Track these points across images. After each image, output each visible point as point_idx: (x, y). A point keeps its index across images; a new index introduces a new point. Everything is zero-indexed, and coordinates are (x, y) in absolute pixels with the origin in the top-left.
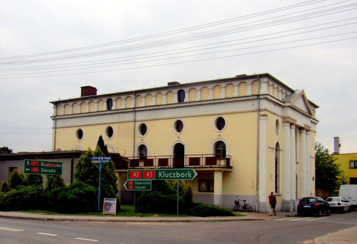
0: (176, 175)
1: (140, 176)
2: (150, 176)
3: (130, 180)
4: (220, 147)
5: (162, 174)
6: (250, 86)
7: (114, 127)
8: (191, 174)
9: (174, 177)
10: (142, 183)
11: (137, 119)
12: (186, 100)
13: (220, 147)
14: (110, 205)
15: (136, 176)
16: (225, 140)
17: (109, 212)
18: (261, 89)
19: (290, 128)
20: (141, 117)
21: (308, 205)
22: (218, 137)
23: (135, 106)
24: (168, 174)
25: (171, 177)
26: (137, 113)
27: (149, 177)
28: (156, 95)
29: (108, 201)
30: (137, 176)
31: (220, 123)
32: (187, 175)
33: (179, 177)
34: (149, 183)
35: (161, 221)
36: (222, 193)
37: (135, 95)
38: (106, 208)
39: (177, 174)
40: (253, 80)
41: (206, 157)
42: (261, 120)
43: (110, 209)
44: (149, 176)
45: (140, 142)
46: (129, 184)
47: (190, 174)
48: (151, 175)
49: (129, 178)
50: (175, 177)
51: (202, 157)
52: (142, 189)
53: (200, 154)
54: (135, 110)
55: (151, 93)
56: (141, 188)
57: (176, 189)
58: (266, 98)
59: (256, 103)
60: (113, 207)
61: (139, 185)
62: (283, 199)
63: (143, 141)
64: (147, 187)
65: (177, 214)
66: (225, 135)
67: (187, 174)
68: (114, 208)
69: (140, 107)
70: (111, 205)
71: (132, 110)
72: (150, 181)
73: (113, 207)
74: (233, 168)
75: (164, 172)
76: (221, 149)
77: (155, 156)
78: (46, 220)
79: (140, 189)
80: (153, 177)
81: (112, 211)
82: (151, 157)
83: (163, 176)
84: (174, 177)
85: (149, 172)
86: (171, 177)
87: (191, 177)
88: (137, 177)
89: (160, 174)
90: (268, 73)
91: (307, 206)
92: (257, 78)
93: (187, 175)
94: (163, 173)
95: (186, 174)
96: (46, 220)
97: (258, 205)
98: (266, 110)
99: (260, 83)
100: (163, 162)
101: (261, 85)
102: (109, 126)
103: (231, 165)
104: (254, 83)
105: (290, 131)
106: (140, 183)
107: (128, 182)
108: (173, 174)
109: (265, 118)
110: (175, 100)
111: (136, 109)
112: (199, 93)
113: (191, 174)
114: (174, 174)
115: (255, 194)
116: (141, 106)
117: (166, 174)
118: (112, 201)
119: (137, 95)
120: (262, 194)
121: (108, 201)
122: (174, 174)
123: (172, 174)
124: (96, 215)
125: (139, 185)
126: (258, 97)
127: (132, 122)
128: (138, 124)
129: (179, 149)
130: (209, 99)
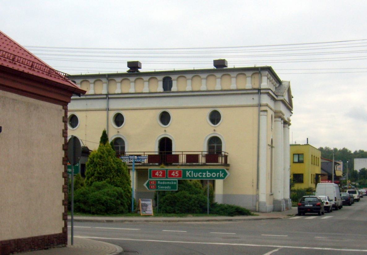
0: (206, 175)
1: (163, 175)
2: (176, 176)
3: (151, 179)
4: (215, 143)
5: (190, 174)
6: (235, 79)
7: (171, 113)
8: (223, 174)
9: (204, 176)
10: (166, 183)
11: (111, 107)
12: (174, 88)
13: (215, 143)
14: (146, 206)
15: (159, 175)
16: (169, 135)
17: (146, 213)
18: (261, 83)
19: (284, 127)
20: (116, 105)
21: (310, 204)
22: (164, 133)
23: (108, 92)
24: (197, 173)
25: (201, 176)
26: (111, 101)
27: (175, 177)
28: (121, 81)
29: (144, 202)
30: (160, 176)
31: (215, 118)
32: (219, 175)
33: (215, 176)
34: (321, 182)
35: (196, 221)
36: (224, 191)
37: (107, 79)
38: (142, 209)
39: (208, 174)
40: (209, 74)
41: (187, 154)
42: (261, 115)
43: (147, 210)
44: (175, 175)
45: (116, 134)
46: (151, 183)
47: (222, 174)
48: (177, 175)
49: (150, 178)
50: (205, 177)
51: (182, 154)
52: (167, 189)
53: (180, 151)
54: (108, 97)
55: (129, 78)
56: (166, 187)
57: (187, 187)
58: (268, 94)
59: (256, 97)
60: (150, 208)
61: (162, 185)
62: (274, 199)
63: (119, 134)
64: (173, 186)
65: (207, 213)
66: (220, 130)
67: (219, 174)
68: (151, 208)
69: (115, 94)
70: (148, 206)
71: (105, 96)
72: (176, 181)
73: (149, 208)
74: (231, 166)
75: (192, 172)
76: (215, 145)
77: (144, 152)
78: (105, 221)
79: (164, 189)
80: (180, 176)
81: (149, 212)
82: (136, 153)
83: (191, 175)
84: (204, 176)
85: (175, 171)
86: (201, 176)
87: (223, 177)
88: (160, 177)
89: (188, 174)
90: (271, 67)
91: (309, 205)
92: (257, 71)
93: (219, 175)
94: (191, 172)
95: (159, 182)
96: (105, 221)
97: (259, 205)
98: (267, 105)
99: (261, 76)
100: (192, 159)
101: (262, 78)
102: (73, 114)
103: (228, 163)
104: (254, 75)
105: (284, 129)
106: (164, 183)
107: (149, 182)
108: (202, 174)
109: (265, 113)
110: (160, 89)
111: (109, 96)
112: (189, 82)
113: (223, 174)
114: (203, 173)
115: (255, 194)
116: (116, 92)
117: (194, 174)
118: (147, 202)
119: (109, 79)
120: (262, 194)
121: (144, 202)
122: (204, 174)
123: (201, 173)
124: (135, 216)
125: (162, 185)
126: (259, 91)
127: (105, 110)
128: (112, 114)
129: (165, 144)
130: (187, 90)
